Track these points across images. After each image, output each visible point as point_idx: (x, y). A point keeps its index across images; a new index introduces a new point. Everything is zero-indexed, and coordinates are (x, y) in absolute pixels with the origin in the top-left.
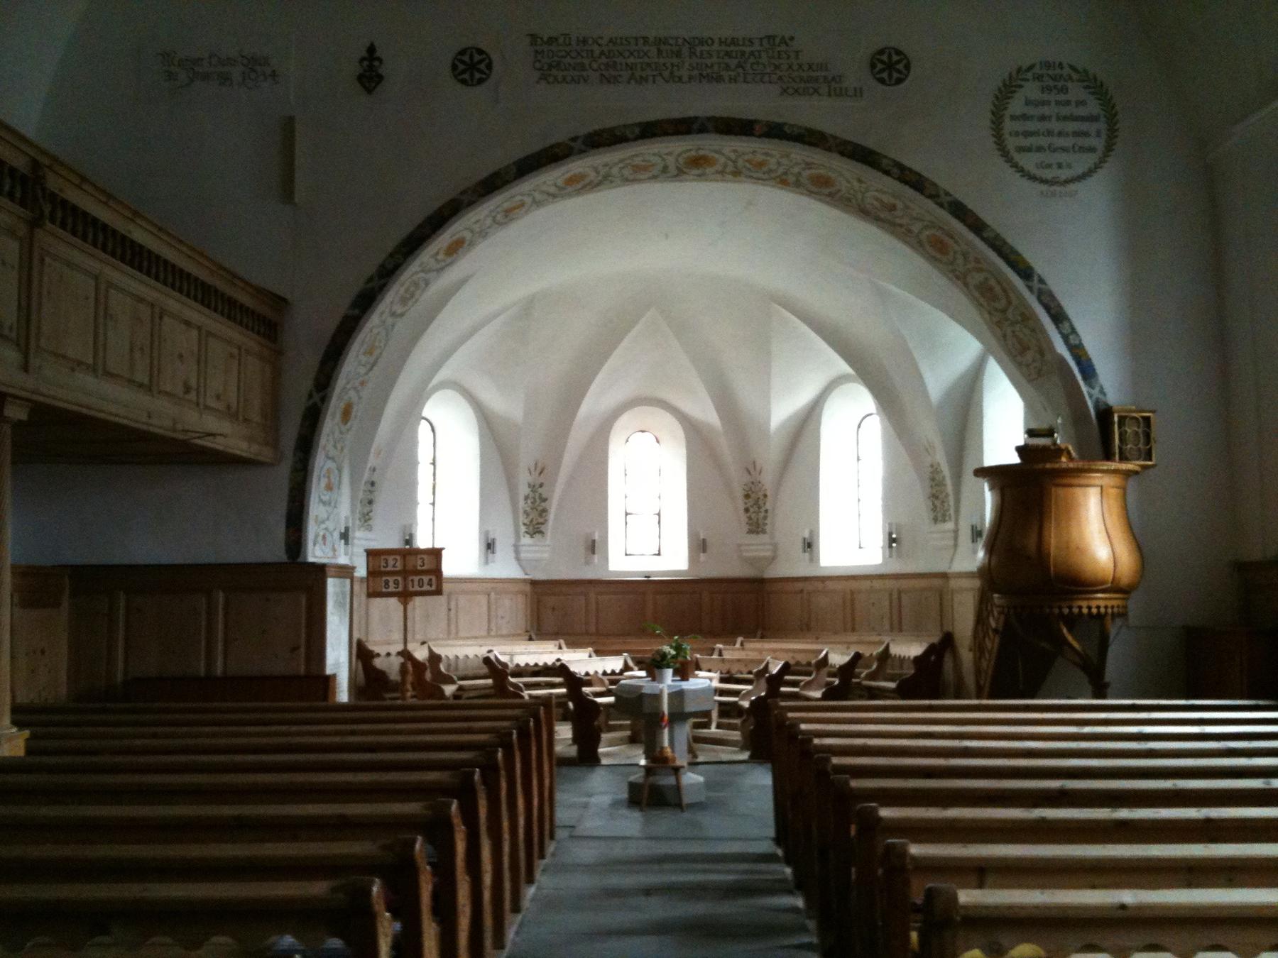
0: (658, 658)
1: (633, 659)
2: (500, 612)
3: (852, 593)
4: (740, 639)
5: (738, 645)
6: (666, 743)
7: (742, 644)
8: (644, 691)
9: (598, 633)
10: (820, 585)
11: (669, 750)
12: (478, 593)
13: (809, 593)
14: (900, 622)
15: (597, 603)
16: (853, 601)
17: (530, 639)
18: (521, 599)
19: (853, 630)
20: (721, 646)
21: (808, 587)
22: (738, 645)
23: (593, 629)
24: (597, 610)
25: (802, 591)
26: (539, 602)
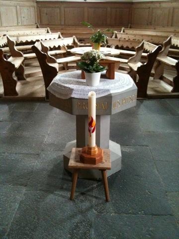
0: (88, 62)
1: (77, 38)
2: (23, 16)
3: (174, 8)
4: (123, 28)
5: (122, 32)
6: (94, 144)
7: (124, 32)
8: (74, 95)
9: (65, 25)
10: (158, 5)
11: (96, 149)
12: (11, 6)
13: (153, 8)
14: (172, 23)
15: (64, 11)
16: (173, 12)
17: (37, 27)
18: (32, 9)
19: (172, 26)
20: (116, 32)
21: (152, 6)
22: (122, 32)
23: (63, 23)
24: (64, 15)
25: (149, 8)
26: (40, 10)
